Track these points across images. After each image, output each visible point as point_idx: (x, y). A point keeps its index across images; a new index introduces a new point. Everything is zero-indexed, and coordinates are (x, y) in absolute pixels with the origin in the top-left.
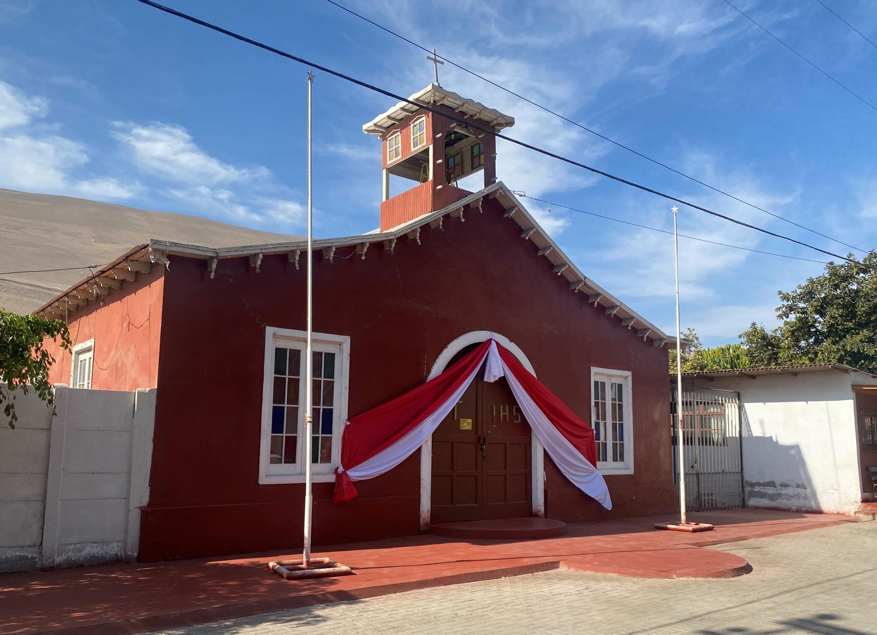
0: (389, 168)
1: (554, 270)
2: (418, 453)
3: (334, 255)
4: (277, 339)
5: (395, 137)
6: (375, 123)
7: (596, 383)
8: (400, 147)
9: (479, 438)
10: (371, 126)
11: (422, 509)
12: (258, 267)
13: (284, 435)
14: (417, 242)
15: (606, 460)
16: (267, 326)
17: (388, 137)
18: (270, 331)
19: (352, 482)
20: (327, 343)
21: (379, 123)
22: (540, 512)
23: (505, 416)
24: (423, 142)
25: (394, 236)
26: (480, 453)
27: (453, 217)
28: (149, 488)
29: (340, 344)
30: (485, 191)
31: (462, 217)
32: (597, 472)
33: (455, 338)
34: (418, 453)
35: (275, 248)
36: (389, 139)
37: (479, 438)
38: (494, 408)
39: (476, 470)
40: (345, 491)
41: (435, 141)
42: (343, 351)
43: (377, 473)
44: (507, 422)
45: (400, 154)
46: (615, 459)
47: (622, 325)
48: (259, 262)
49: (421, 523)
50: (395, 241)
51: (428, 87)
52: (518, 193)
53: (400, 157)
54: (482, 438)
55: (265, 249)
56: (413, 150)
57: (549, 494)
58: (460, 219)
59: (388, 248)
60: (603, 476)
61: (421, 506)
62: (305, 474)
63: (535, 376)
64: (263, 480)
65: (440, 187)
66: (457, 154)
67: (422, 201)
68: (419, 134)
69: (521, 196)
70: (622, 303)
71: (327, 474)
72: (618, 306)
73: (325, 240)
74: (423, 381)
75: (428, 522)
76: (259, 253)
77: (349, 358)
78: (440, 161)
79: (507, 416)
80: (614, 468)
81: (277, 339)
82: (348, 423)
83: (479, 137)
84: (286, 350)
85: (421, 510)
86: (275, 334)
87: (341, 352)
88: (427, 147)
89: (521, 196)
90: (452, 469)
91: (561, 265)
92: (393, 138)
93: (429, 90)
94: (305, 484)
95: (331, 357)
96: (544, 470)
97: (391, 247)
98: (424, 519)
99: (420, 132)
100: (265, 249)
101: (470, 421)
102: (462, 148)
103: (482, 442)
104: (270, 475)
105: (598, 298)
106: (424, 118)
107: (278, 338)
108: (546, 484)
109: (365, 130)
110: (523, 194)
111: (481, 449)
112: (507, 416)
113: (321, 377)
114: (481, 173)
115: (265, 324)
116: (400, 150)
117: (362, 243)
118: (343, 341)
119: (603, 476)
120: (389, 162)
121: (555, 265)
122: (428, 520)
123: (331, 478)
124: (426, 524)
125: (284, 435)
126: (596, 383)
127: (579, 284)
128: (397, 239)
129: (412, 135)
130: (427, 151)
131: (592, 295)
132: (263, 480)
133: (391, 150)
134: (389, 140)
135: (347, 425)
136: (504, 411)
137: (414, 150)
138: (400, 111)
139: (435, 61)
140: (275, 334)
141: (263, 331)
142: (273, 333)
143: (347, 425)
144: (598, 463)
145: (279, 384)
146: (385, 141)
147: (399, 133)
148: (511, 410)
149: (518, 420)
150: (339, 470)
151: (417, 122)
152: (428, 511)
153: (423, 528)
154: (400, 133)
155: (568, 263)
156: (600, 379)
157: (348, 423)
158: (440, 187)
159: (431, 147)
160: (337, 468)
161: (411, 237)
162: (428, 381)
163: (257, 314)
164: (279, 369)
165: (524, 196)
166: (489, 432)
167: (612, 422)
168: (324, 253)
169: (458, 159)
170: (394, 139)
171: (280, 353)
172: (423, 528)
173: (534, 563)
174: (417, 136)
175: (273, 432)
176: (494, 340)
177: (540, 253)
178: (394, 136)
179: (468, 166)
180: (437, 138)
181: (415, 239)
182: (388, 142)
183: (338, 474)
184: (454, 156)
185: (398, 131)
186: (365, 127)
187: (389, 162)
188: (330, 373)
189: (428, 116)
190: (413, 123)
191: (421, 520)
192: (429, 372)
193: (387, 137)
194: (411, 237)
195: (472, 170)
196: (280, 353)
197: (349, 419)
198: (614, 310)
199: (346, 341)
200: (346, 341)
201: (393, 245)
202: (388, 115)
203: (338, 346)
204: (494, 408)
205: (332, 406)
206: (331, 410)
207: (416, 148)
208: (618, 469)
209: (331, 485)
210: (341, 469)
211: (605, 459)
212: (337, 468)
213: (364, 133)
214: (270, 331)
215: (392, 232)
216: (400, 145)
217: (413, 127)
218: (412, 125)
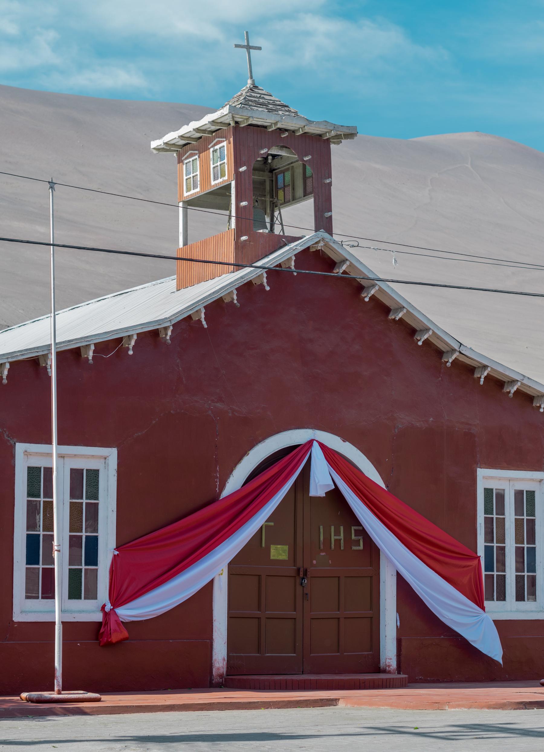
0: (187, 201)
1: (415, 337)
2: (209, 587)
3: (94, 353)
4: (29, 456)
5: (193, 161)
6: (165, 142)
7: (488, 492)
8: (198, 176)
9: (299, 570)
10: (161, 145)
11: (215, 657)
12: (5, 377)
13: (41, 566)
14: (203, 325)
15: (504, 599)
16: (17, 442)
17: (186, 159)
18: (20, 448)
19: (122, 622)
20: (88, 458)
21: (171, 142)
22: (389, 666)
23: (338, 541)
24: (225, 176)
25: (169, 322)
26: (299, 589)
27: (255, 284)
28: (347, 443)
29: (105, 458)
30: (298, 247)
31: (265, 284)
32: (485, 615)
33: (260, 442)
34: (209, 587)
35: (23, 355)
36: (185, 162)
37: (299, 570)
38: (322, 530)
39: (295, 611)
40: (112, 631)
41: (238, 176)
42: (108, 466)
43: (157, 611)
44: (342, 548)
45: (199, 186)
46: (520, 597)
47: (534, 405)
48: (6, 372)
49: (214, 674)
50: (171, 328)
51: (225, 108)
52: (347, 243)
53: (198, 190)
54: (302, 570)
55: (12, 358)
56: (213, 183)
57: (403, 643)
58: (264, 287)
59: (164, 336)
60: (494, 621)
61: (214, 654)
62: (55, 612)
63: (383, 486)
64: (18, 617)
65: (244, 238)
66: (288, 170)
67: (223, 255)
68: (219, 163)
69: (353, 246)
70: (524, 376)
71: (93, 612)
72: (518, 381)
73: (81, 338)
74: (214, 499)
75: (223, 674)
76: (5, 363)
77: (116, 475)
78: (244, 204)
79: (342, 541)
80: (517, 611)
81: (29, 456)
82: (116, 553)
83: (305, 159)
84: (40, 468)
85: (214, 658)
86: (26, 451)
87: (107, 467)
88: (230, 182)
89: (353, 246)
90: (259, 609)
91: (424, 330)
92: (190, 162)
93: (225, 113)
94: (54, 623)
95: (94, 475)
96: (397, 612)
97: (166, 335)
98: (218, 669)
99: (220, 162)
100: (12, 358)
101: (286, 548)
102: (292, 163)
103: (301, 576)
104: (25, 612)
105: (485, 370)
106: (225, 144)
107: (31, 455)
108: (399, 631)
109: (154, 148)
110: (356, 244)
111: (301, 584)
112: (342, 541)
113: (82, 498)
114: (309, 204)
115: (15, 440)
116: (199, 179)
117: (129, 336)
118: (108, 455)
119: (494, 621)
120: (186, 194)
121: (418, 329)
122: (224, 670)
123: (98, 617)
124: (221, 676)
125: (41, 566)
126: (488, 492)
127: (452, 354)
128: (174, 325)
129: (211, 163)
130: (228, 187)
131: (479, 367)
132: (18, 617)
133: (188, 177)
134: (186, 163)
135: (115, 555)
136: (337, 533)
137: (215, 183)
138: (194, 133)
139: (248, 47)
140: (26, 451)
141: (13, 447)
142: (24, 450)
143: (115, 555)
144: (486, 603)
145: (32, 509)
146: (181, 164)
147: (197, 157)
148: (347, 533)
149: (359, 546)
150: (106, 608)
151: (217, 147)
152: (224, 660)
153: (216, 679)
154: (199, 157)
155: (431, 328)
156: (494, 485)
157: (116, 553)
158: (244, 238)
159: (233, 184)
160: (104, 606)
161: (195, 318)
162: (222, 498)
163: (5, 429)
164: (32, 492)
165: (358, 246)
166: (315, 562)
167: (515, 545)
168: (82, 351)
169: (288, 175)
170: (191, 163)
171: (33, 472)
172: (216, 679)
173: (229, 701)
174: (217, 166)
175: (28, 563)
176: (317, 441)
177: (391, 317)
178: (191, 160)
179: (300, 192)
180: (241, 173)
181: (199, 321)
182: (184, 166)
183: (106, 612)
184: (283, 172)
185: (196, 154)
186: (154, 144)
187: (186, 194)
188: (94, 494)
189: (230, 143)
190: (212, 147)
191: (214, 670)
192: (222, 487)
193: (183, 159)
194: (195, 318)
195: (304, 196)
196: (33, 472)
197: (117, 549)
198: (514, 386)
199: (112, 453)
200: (112, 453)
201: (169, 333)
202: (180, 135)
203: (103, 461)
204: (322, 530)
205: (97, 533)
206: (96, 538)
207: (217, 182)
208: (523, 612)
209: (99, 624)
210: (109, 607)
211: (502, 597)
212: (104, 606)
213: (153, 152)
214: (20, 448)
215: (166, 318)
216: (198, 173)
217: (213, 151)
218: (212, 150)
